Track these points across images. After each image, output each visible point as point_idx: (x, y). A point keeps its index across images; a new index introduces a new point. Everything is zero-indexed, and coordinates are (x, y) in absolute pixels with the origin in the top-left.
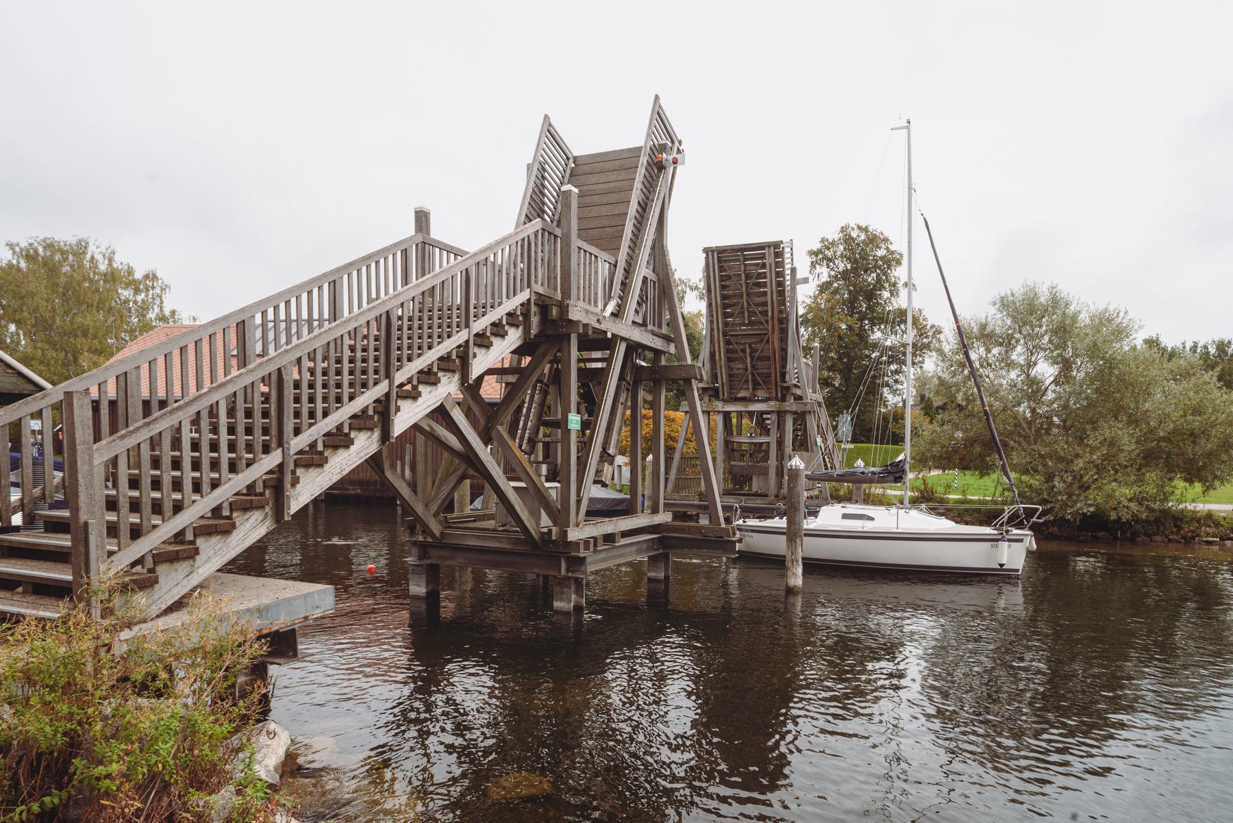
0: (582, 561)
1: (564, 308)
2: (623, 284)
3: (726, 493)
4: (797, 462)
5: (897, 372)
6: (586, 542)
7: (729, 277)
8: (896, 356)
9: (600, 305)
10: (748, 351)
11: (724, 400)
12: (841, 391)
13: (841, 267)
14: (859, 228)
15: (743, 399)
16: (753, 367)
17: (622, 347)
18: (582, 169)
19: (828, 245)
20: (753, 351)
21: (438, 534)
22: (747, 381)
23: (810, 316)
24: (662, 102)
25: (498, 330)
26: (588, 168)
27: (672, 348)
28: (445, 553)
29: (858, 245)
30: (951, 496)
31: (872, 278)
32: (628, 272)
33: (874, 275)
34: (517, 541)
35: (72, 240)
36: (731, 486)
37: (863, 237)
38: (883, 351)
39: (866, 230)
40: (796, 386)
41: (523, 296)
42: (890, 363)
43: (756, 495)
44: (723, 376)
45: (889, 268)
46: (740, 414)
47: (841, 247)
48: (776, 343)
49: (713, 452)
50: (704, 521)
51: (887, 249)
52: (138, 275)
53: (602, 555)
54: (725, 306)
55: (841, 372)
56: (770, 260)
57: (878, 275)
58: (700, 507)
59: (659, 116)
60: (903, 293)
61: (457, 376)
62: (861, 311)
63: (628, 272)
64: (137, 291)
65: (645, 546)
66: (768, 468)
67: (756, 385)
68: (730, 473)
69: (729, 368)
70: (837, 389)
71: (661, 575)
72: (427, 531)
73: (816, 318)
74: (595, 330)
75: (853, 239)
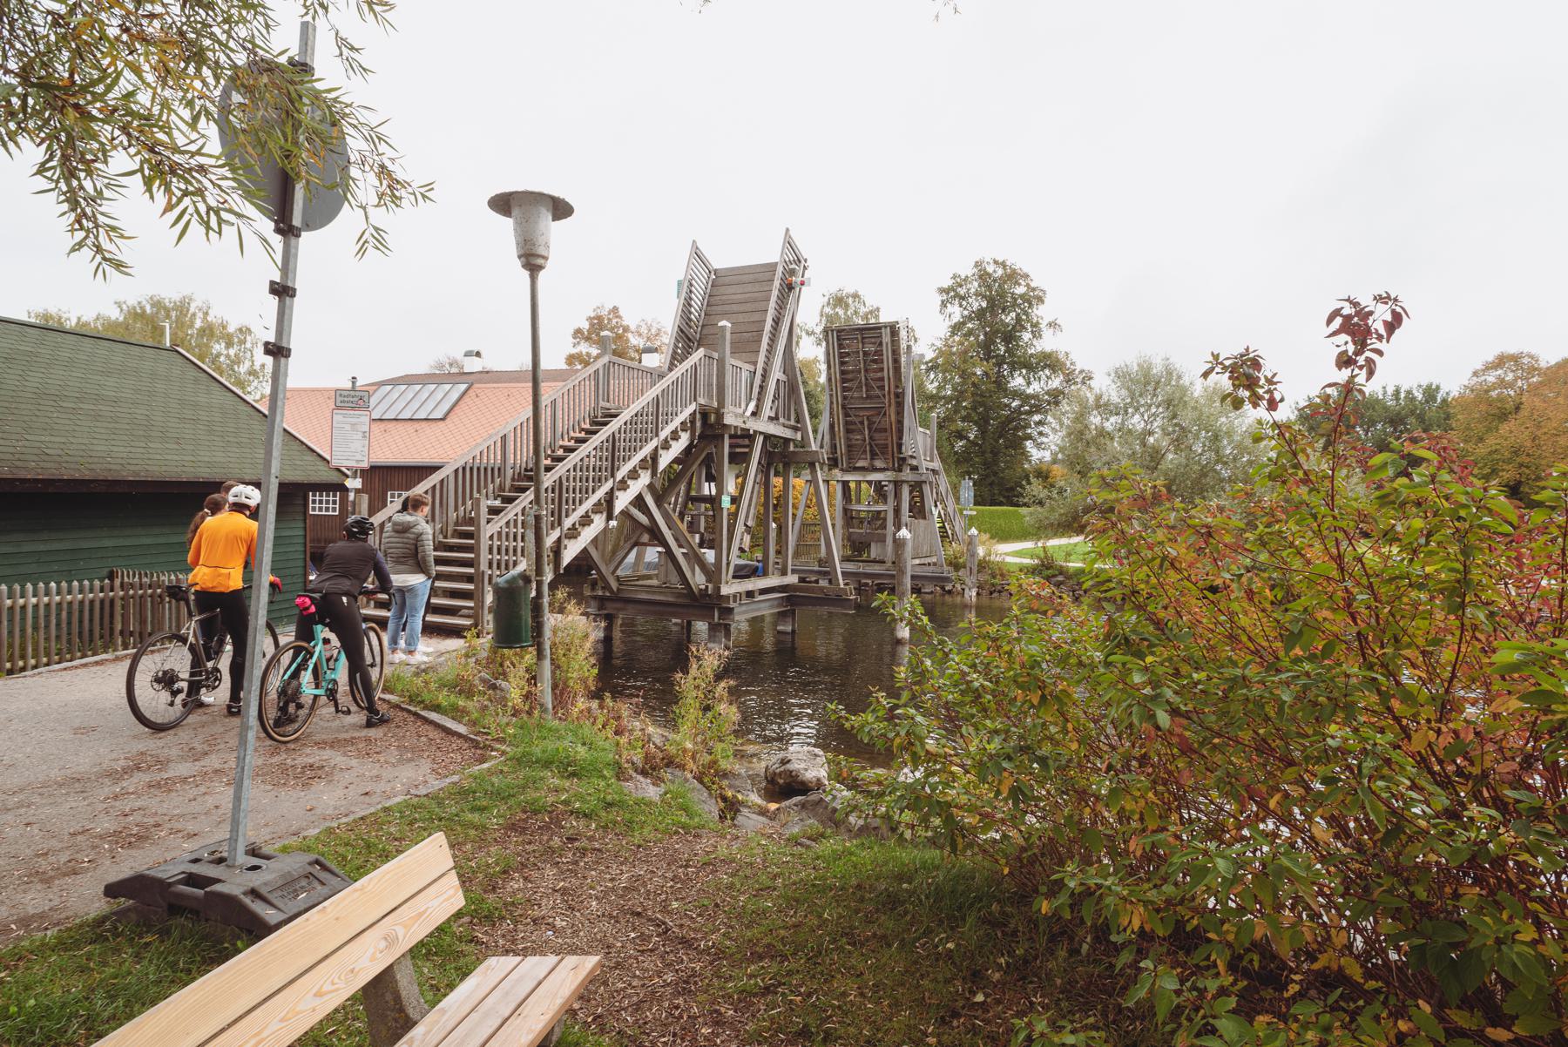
0: (731, 610)
1: (720, 416)
2: (761, 387)
3: (845, 559)
4: (904, 533)
5: (1040, 423)
6: (735, 596)
7: (848, 354)
8: (1037, 405)
9: (743, 406)
10: (866, 423)
11: (842, 470)
12: (977, 444)
13: (976, 306)
14: (996, 262)
15: (863, 469)
16: (871, 438)
17: (760, 440)
18: (721, 281)
19: (960, 282)
20: (871, 424)
21: (615, 589)
22: (865, 451)
23: (940, 361)
24: (791, 233)
25: (675, 436)
26: (727, 280)
27: (799, 436)
28: (618, 605)
29: (995, 281)
30: (1071, 564)
31: (1009, 318)
32: (765, 376)
33: (1013, 315)
34: (679, 595)
35: (176, 297)
36: (849, 553)
37: (1000, 272)
38: (1026, 398)
39: (1003, 265)
40: (912, 457)
41: (692, 408)
42: (1030, 413)
43: (874, 561)
44: (842, 447)
45: (1031, 306)
46: (858, 483)
47: (976, 284)
48: (893, 418)
49: (833, 518)
50: (823, 583)
51: (1028, 285)
52: (231, 329)
53: (744, 608)
54: (844, 381)
55: (976, 423)
56: (886, 339)
57: (1018, 315)
58: (819, 573)
59: (789, 243)
60: (1047, 333)
61: (649, 472)
62: (998, 356)
63: (765, 376)
64: (229, 345)
65: (776, 603)
66: (885, 535)
67: (873, 456)
68: (849, 540)
69: (848, 439)
70: (974, 443)
71: (789, 629)
72: (607, 587)
73: (944, 363)
74: (742, 429)
75: (990, 275)
